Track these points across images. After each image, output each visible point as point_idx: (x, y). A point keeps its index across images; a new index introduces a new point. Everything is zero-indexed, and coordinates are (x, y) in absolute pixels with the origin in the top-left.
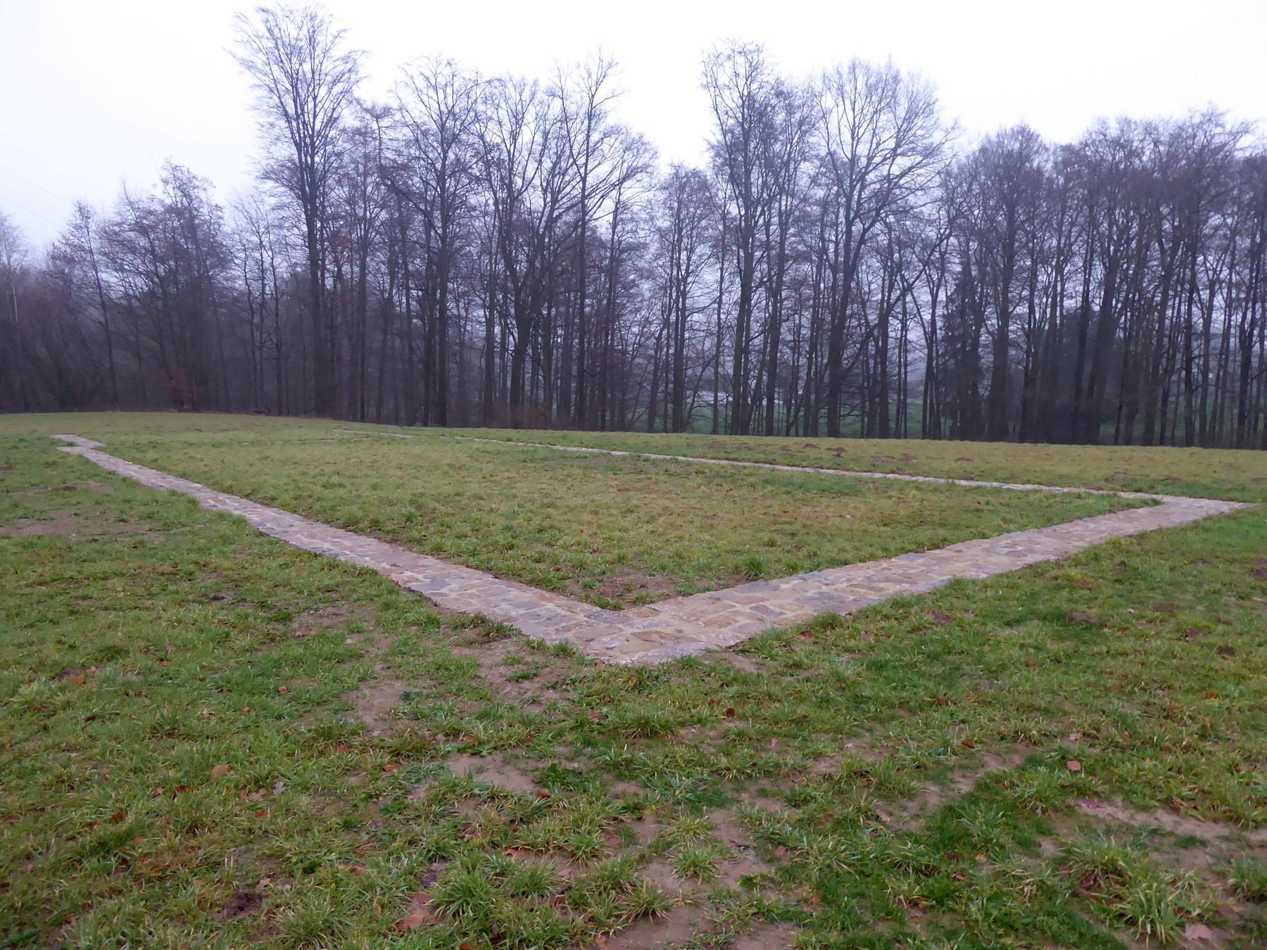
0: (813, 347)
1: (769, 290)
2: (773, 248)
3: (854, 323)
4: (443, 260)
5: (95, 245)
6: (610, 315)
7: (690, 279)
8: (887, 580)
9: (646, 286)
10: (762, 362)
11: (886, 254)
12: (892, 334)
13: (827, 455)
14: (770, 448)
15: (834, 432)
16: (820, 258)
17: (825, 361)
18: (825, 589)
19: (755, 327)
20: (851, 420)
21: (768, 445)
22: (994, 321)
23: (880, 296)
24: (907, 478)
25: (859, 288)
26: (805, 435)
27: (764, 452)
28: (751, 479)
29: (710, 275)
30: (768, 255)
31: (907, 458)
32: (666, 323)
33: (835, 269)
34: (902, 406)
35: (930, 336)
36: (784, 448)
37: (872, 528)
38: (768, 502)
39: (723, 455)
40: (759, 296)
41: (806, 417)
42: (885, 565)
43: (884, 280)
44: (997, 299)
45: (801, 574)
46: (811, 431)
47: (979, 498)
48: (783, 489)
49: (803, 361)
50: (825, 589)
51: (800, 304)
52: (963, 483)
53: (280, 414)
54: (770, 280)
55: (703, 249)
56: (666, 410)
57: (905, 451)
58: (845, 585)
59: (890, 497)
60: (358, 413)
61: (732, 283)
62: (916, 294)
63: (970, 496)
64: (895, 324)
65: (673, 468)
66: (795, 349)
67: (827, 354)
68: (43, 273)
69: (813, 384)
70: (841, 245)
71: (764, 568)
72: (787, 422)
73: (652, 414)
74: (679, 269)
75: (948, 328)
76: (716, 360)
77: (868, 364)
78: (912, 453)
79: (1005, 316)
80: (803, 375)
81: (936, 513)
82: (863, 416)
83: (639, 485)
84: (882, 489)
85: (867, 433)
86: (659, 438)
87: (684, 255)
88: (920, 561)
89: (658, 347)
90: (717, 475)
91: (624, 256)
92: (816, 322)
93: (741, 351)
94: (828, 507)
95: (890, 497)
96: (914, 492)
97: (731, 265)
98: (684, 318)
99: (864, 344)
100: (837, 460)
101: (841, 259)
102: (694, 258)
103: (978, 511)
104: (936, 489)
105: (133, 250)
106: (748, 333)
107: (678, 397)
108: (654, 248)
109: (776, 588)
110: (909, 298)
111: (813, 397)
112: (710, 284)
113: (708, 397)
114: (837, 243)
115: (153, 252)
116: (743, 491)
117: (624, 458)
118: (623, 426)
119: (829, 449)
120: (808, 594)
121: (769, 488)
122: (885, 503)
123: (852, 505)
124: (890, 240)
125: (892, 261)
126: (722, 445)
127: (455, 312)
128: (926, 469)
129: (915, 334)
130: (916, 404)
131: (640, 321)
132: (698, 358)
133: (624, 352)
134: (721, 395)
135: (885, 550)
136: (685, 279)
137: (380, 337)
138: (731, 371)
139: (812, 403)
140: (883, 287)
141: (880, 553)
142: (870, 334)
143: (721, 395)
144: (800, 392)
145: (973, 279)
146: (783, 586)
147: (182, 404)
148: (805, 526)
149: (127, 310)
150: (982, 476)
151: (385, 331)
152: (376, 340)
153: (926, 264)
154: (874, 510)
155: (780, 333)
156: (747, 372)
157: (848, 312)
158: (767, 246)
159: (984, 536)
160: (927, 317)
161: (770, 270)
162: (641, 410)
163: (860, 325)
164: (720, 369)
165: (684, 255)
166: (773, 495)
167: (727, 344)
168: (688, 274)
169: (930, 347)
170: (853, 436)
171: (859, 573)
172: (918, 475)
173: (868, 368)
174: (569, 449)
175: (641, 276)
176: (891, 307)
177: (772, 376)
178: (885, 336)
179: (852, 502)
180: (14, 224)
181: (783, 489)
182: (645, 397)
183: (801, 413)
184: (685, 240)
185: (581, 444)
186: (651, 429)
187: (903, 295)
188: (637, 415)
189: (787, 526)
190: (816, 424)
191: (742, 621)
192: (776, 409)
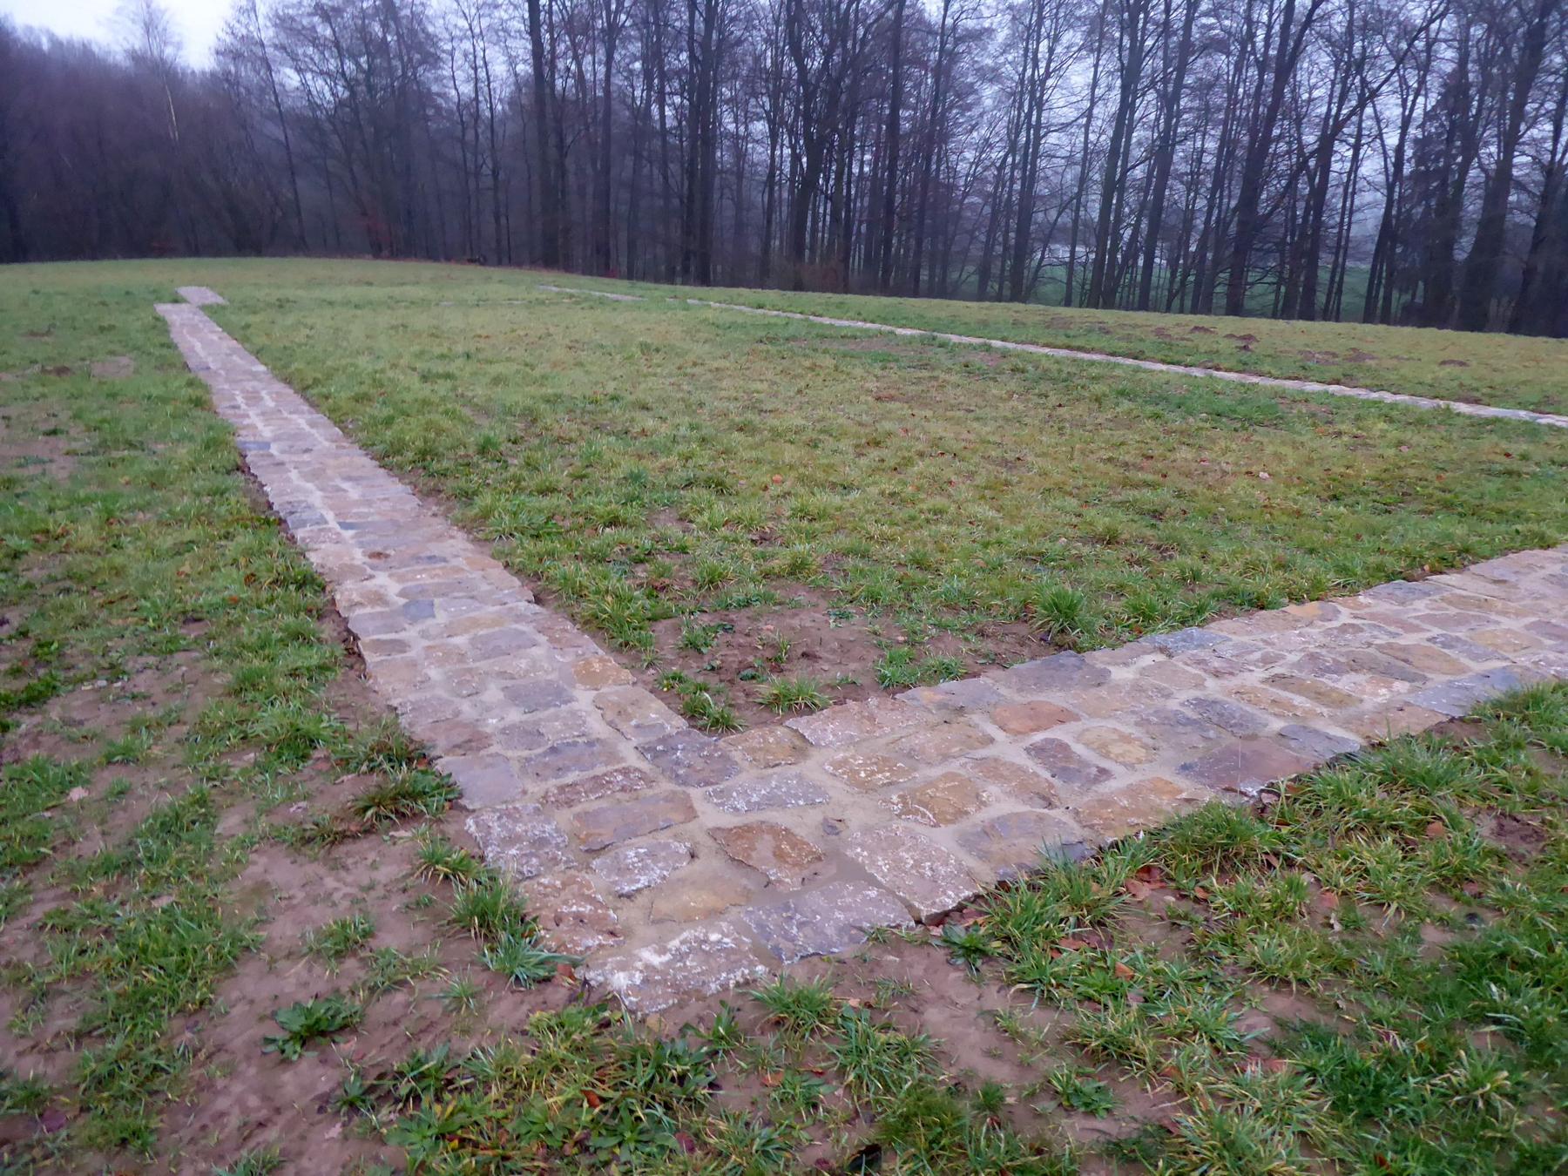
0: (1218, 184)
1: (1162, 96)
2: (1175, 33)
3: (1283, 147)
4: (712, 57)
5: (268, 34)
6: (934, 135)
7: (1050, 82)
8: (1355, 665)
9: (988, 93)
10: (1143, 205)
11: (1340, 47)
12: (1336, 167)
13: (1226, 346)
14: (1138, 332)
15: (1235, 308)
16: (1243, 51)
17: (1233, 203)
18: (1213, 687)
19: (1137, 153)
20: (1261, 290)
21: (1135, 326)
22: (1493, 149)
23: (1324, 109)
24: (1363, 394)
25: (1295, 99)
26: (1194, 311)
27: (1128, 338)
28: (1098, 388)
29: (1079, 75)
30: (1166, 45)
31: (1357, 356)
32: (1012, 148)
33: (1262, 67)
34: (1338, 270)
35: (1395, 176)
36: (1160, 332)
37: (1310, 504)
38: (1119, 435)
39: (1062, 340)
40: (1147, 107)
41: (1198, 283)
42: (1345, 617)
43: (1333, 83)
44: (1501, 115)
45: (1161, 636)
46: (1202, 305)
47: (1504, 445)
48: (1150, 409)
49: (1201, 203)
50: (1213, 687)
51: (1206, 112)
52: (1464, 408)
53: (499, 263)
54: (1165, 81)
55: (1073, 37)
56: (1003, 270)
57: (1354, 344)
58: (1260, 674)
59: (1339, 434)
60: (602, 264)
61: (1110, 88)
62: (1378, 108)
63: (1487, 442)
64: (1343, 150)
65: (977, 359)
66: (1193, 185)
67: (1237, 192)
68: (213, 74)
69: (1212, 237)
70: (1277, 28)
71: (1083, 615)
72: (1170, 291)
73: (984, 273)
74: (1036, 66)
75: (1420, 158)
76: (1078, 201)
77: (1294, 209)
78: (1366, 348)
79: (1510, 142)
80: (1199, 223)
81: (1431, 475)
82: (1278, 284)
83: (912, 390)
84: (1326, 416)
85: (1284, 310)
86: (972, 310)
87: (1044, 46)
88: (1421, 606)
89: (999, 179)
90: (1045, 376)
91: (961, 48)
92: (1226, 142)
93: (1113, 186)
94: (1226, 450)
95: (1339, 434)
96: (1382, 425)
97: (1110, 62)
98: (1038, 138)
99: (1293, 179)
100: (1244, 356)
101: (1273, 52)
102: (1059, 49)
103: (1510, 473)
104: (1419, 422)
105: (315, 41)
106: (1125, 161)
107: (1021, 252)
108: (1002, 35)
109: (1100, 679)
110: (1369, 110)
111: (1210, 256)
112: (1078, 86)
113: (1063, 252)
114: (1270, 27)
115: (337, 44)
116: (1081, 409)
117: (910, 341)
118: (942, 290)
119: (1231, 336)
120: (1173, 705)
121: (1126, 405)
122: (1332, 448)
123: (1269, 449)
124: (1351, 22)
125: (1350, 55)
126: (1066, 324)
127: (732, 127)
128: (1393, 377)
129: (1372, 167)
130: (1359, 270)
131: (975, 146)
132: (1052, 195)
133: (951, 187)
134: (1080, 249)
135: (1343, 570)
136: (1043, 82)
137: (629, 161)
138: (1095, 215)
139: (1208, 264)
140: (1331, 96)
141: (1331, 578)
142: (1303, 165)
143: (1080, 249)
144: (1193, 248)
145: (1469, 85)
146: (1120, 674)
147: (380, 249)
148: (1180, 495)
149: (307, 122)
150: (1492, 399)
151: (637, 155)
152: (624, 168)
153: (1400, 59)
154: (1310, 462)
155: (1170, 162)
156: (1119, 220)
157: (1276, 132)
158: (1166, 28)
159: (1546, 544)
160: (1392, 139)
161: (1166, 66)
162: (971, 268)
163: (1289, 152)
164: (1082, 213)
165: (1044, 46)
166: (1131, 421)
167: (1097, 177)
168: (1048, 75)
169: (1390, 188)
170: (1262, 315)
171: (1294, 634)
172: (1381, 388)
173: (1295, 217)
174: (838, 323)
175: (983, 78)
176: (1339, 125)
177: (1155, 226)
178: (1325, 167)
179: (1271, 442)
180: (163, 7)
181: (1150, 409)
182: (976, 251)
183: (1192, 278)
184: (1047, 23)
185: (859, 316)
186: (981, 296)
187: (1362, 105)
188: (964, 276)
189: (1147, 493)
190: (1210, 295)
191: (1000, 803)
192: (1155, 271)
